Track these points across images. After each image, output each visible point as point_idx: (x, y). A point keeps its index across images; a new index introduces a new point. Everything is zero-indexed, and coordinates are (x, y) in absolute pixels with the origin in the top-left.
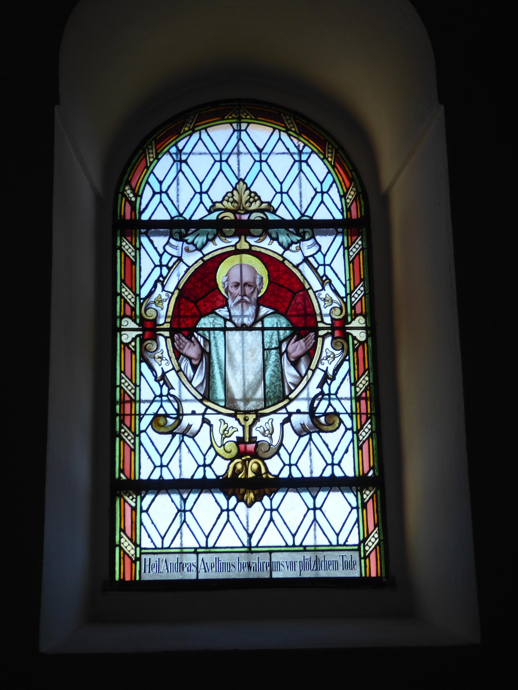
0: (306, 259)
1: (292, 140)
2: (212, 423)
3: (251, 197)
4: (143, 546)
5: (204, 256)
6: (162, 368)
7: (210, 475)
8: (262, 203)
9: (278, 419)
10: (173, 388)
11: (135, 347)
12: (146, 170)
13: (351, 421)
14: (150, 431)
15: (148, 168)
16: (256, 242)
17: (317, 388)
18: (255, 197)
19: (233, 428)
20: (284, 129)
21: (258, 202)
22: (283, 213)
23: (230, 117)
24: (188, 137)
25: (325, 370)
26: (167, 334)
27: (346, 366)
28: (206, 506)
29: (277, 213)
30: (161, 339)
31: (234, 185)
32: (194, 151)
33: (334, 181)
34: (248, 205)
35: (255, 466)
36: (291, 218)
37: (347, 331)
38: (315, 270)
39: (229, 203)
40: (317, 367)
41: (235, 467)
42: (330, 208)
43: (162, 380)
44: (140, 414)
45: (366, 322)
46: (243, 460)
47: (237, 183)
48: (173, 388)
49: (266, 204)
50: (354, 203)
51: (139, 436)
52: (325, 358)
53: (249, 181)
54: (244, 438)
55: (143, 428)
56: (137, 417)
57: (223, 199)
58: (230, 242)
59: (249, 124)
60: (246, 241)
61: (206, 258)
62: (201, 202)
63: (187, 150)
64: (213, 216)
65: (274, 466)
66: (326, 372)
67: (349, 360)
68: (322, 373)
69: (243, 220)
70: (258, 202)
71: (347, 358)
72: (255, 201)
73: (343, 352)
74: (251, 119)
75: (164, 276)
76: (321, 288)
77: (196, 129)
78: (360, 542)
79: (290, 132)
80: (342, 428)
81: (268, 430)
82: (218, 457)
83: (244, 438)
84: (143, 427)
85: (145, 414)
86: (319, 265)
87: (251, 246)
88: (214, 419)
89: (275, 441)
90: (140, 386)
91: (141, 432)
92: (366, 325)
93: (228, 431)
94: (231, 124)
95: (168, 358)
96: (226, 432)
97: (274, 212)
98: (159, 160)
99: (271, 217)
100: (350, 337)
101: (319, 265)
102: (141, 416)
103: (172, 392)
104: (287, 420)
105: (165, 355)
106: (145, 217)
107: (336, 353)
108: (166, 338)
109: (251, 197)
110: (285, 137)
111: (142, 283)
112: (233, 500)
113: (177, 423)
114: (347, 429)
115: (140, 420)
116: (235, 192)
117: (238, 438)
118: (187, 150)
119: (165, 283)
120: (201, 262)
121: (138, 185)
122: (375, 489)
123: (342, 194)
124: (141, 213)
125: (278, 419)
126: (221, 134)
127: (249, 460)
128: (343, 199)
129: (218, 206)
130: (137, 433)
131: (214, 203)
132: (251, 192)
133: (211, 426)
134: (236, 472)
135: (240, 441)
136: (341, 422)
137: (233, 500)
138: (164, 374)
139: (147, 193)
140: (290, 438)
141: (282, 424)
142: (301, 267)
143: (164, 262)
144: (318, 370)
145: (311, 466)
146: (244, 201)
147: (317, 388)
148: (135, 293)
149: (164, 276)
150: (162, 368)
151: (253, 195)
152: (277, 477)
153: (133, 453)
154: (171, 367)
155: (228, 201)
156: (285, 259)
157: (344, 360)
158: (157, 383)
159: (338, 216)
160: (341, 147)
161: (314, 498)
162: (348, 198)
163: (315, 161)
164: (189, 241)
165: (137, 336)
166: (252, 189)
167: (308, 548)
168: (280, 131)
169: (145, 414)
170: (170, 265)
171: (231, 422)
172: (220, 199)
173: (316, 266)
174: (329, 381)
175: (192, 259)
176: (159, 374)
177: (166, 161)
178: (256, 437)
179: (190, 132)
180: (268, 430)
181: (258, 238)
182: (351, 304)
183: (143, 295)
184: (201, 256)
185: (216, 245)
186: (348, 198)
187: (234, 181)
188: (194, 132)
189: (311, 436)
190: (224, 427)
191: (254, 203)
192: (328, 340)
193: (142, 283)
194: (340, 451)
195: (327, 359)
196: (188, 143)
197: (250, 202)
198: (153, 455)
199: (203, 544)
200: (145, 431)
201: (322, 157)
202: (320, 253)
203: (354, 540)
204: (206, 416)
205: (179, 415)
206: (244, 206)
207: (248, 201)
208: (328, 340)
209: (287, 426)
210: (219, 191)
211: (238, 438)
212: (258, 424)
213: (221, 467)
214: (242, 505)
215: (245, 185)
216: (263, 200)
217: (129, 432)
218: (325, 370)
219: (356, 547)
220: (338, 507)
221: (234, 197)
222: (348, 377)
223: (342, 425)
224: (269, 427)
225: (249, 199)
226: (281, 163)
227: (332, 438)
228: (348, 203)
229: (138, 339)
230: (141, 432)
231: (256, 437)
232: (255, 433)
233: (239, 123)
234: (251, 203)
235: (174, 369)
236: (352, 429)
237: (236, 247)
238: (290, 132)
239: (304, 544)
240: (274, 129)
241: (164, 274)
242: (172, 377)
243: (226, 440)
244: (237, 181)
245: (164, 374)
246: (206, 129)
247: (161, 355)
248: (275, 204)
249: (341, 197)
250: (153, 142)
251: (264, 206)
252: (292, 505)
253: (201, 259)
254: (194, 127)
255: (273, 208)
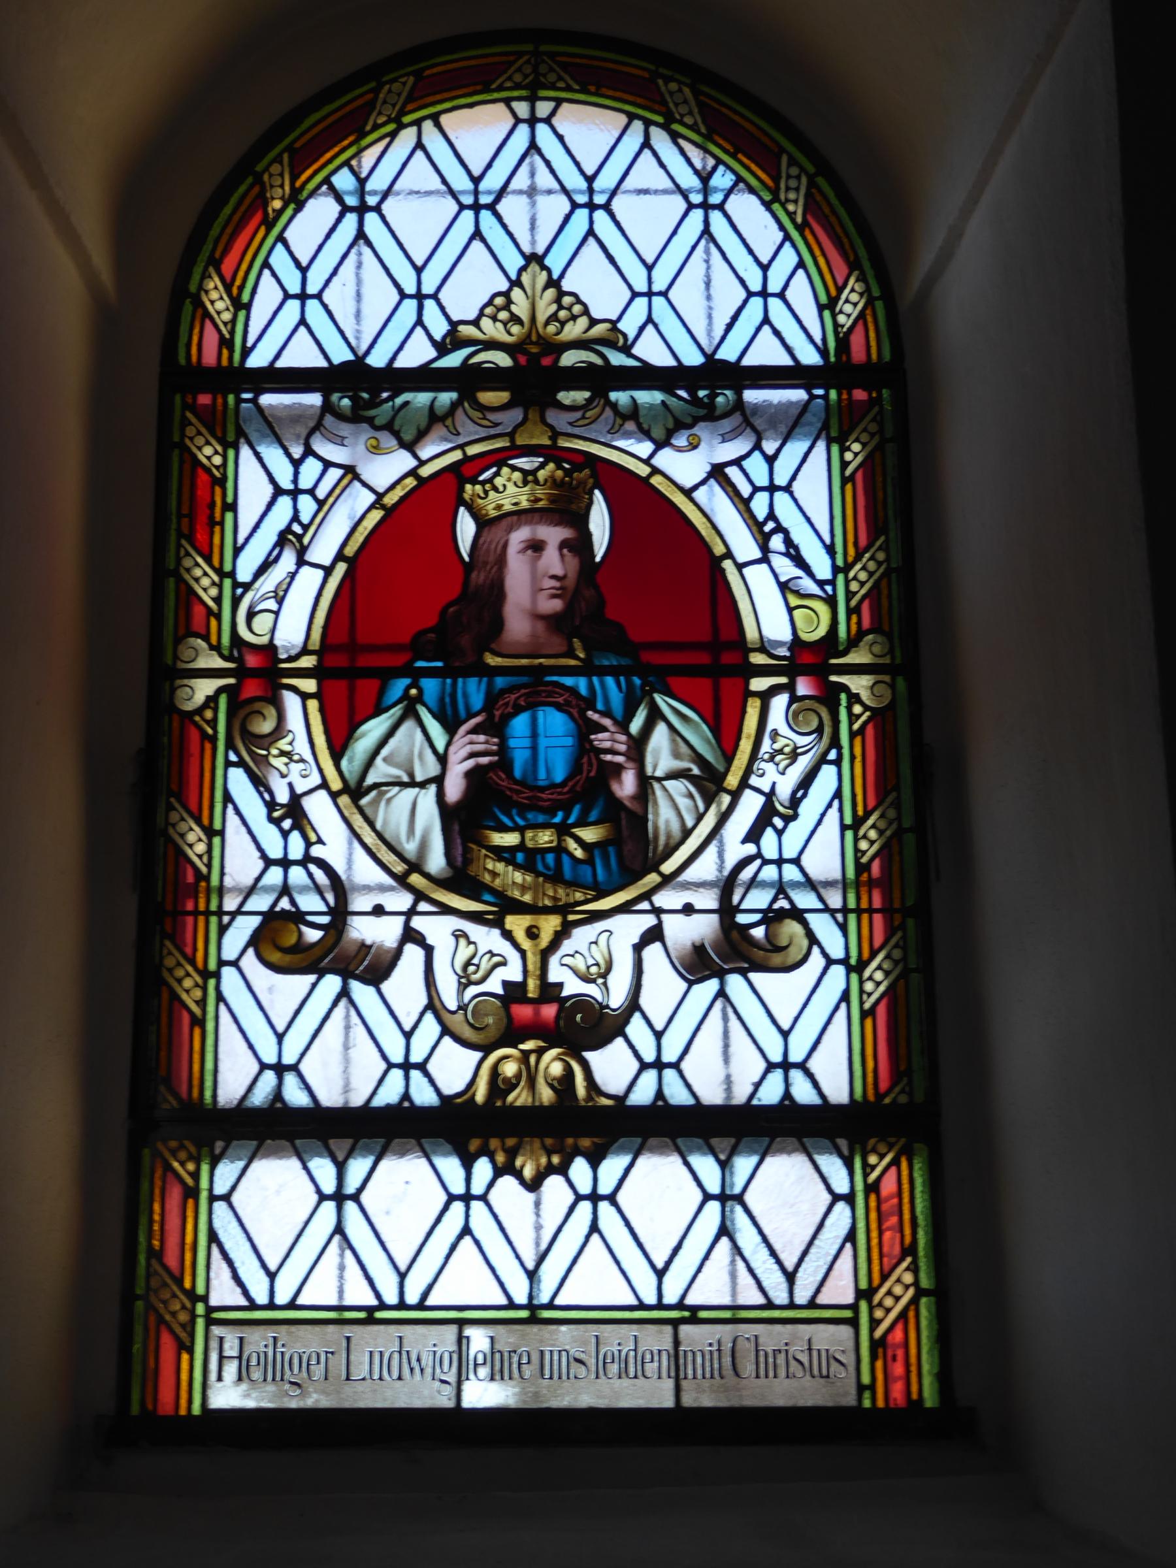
0: (717, 472)
1: (682, 152)
2: (429, 941)
3: (560, 307)
4: (214, 1302)
5: (422, 463)
6: (290, 785)
7: (424, 1096)
8: (594, 322)
9: (633, 926)
10: (320, 841)
11: (213, 723)
12: (185, 1357)
13: (842, 940)
14: (250, 960)
15: (270, 226)
16: (571, 424)
17: (744, 842)
18: (572, 305)
19: (494, 955)
20: (660, 119)
21: (583, 322)
22: (651, 351)
23: (508, 84)
24: (387, 140)
25: (767, 789)
26: (309, 685)
27: (828, 777)
28: (405, 1188)
29: (635, 351)
30: (292, 702)
31: (513, 276)
32: (397, 187)
33: (801, 264)
34: (551, 329)
35: (557, 1069)
36: (672, 362)
37: (833, 678)
38: (743, 504)
39: (499, 325)
40: (744, 784)
41: (495, 1072)
42: (793, 323)
43: (292, 814)
44: (220, 913)
45: (891, 652)
46: (522, 1051)
47: (522, 270)
48: (320, 841)
49: (607, 325)
50: (860, 328)
51: (217, 975)
52: (766, 756)
53: (556, 262)
54: (523, 985)
55: (229, 953)
56: (214, 920)
57: (481, 314)
58: (496, 425)
59: (559, 102)
60: (544, 422)
61: (425, 471)
62: (419, 322)
63: (378, 183)
64: (453, 360)
65: (611, 1067)
66: (770, 796)
67: (838, 762)
68: (760, 800)
69: (538, 377)
70: (583, 322)
71: (832, 755)
72: (574, 318)
73: (821, 738)
74: (568, 89)
75: (305, 520)
76: (758, 554)
77: (407, 119)
78: (860, 1294)
79: (676, 127)
80: (816, 961)
81: (597, 964)
82: (745, 463)
83: (523, 985)
84: (230, 950)
85: (239, 912)
86: (756, 489)
87: (555, 434)
88: (437, 929)
89: (617, 998)
90: (222, 833)
91: (222, 963)
92: (893, 658)
93: (478, 966)
94: (507, 102)
95: (308, 756)
96: (471, 969)
97: (627, 350)
98: (300, 207)
99: (617, 359)
100: (843, 696)
101: (756, 489)
102: (226, 919)
103: (316, 851)
104: (654, 935)
105: (302, 747)
106: (257, 360)
107: (802, 741)
108: (304, 696)
109: (560, 307)
110: (660, 139)
111: (241, 541)
112: (483, 1169)
113: (330, 941)
114: (830, 962)
115: (223, 929)
116: (517, 294)
117: (506, 984)
118: (378, 183)
119: (306, 541)
120: (411, 482)
121: (241, 274)
122: (903, 1141)
123: (823, 299)
124: (246, 352)
125: (633, 926)
126: (478, 132)
127: (540, 1052)
128: (827, 314)
129: (467, 331)
130: (212, 965)
131: (454, 325)
132: (561, 293)
133: (429, 950)
134: (499, 1086)
135: (514, 992)
136: (813, 940)
137: (483, 1169)
138: (296, 799)
139: (267, 296)
140: (662, 985)
141: (638, 948)
142: (699, 495)
143: (305, 482)
144: (748, 792)
145: (714, 1074)
146: (541, 317)
147: (744, 842)
148: (220, 572)
149: (305, 520)
150: (290, 785)
151: (567, 300)
152: (620, 1099)
153: (208, 746)
154: (316, 779)
155: (494, 319)
156: (656, 471)
157: (822, 760)
158: (273, 829)
159: (809, 357)
160: (824, 168)
161: (725, 1165)
162: (841, 312)
163: (748, 209)
164: (378, 422)
165: (220, 691)
166: (566, 285)
167: (703, 1314)
168: (648, 123)
169: (239, 912)
170: (321, 493)
171: (488, 939)
172: (472, 315)
173: (745, 490)
174: (778, 822)
175: (389, 468)
176: (283, 797)
177: (320, 211)
178: (560, 985)
179: (391, 127)
180: (597, 964)
181: (578, 414)
182: (848, 600)
183: (244, 576)
184: (413, 463)
185: (458, 434)
186: (841, 312)
187: (514, 262)
188: (402, 126)
189: (722, 984)
190: (465, 952)
191: (571, 322)
192: (779, 703)
193: (241, 541)
194: (806, 1024)
195: (772, 759)
196: (387, 161)
197: (558, 320)
198: (261, 1028)
199: (391, 1298)
200: (235, 964)
201: (767, 197)
202: (757, 454)
203: (841, 1290)
204: (417, 923)
205: (340, 913)
206: (540, 330)
207: (554, 317)
208: (779, 703)
209: (653, 952)
210: (470, 289)
211: (506, 984)
212: (567, 946)
213: (455, 1069)
214: (508, 1182)
215: (544, 273)
216: (596, 314)
217: (175, 1288)
218: (767, 789)
219: (848, 1314)
220: (792, 1193)
221: (513, 308)
222: (836, 803)
223: (816, 950)
224: (601, 952)
225: (555, 314)
226: (649, 217)
227: (781, 990)
228: (843, 326)
229: (223, 701)
230: (222, 963)
231: (560, 985)
232: (556, 974)
233: (532, 100)
234: (563, 324)
235: (324, 785)
236: (844, 962)
237: (512, 441)
238: (676, 127)
239: (690, 1300)
240: (632, 117)
241: (305, 518)
242: (319, 808)
243: (472, 991)
244: (522, 262)
245: (296, 799)
246: (435, 118)
247: (288, 748)
248: (629, 326)
249: (821, 308)
250: (286, 156)
251: (599, 330)
252: (660, 1188)
253: (413, 473)
254: (403, 113)
255: (625, 336)
